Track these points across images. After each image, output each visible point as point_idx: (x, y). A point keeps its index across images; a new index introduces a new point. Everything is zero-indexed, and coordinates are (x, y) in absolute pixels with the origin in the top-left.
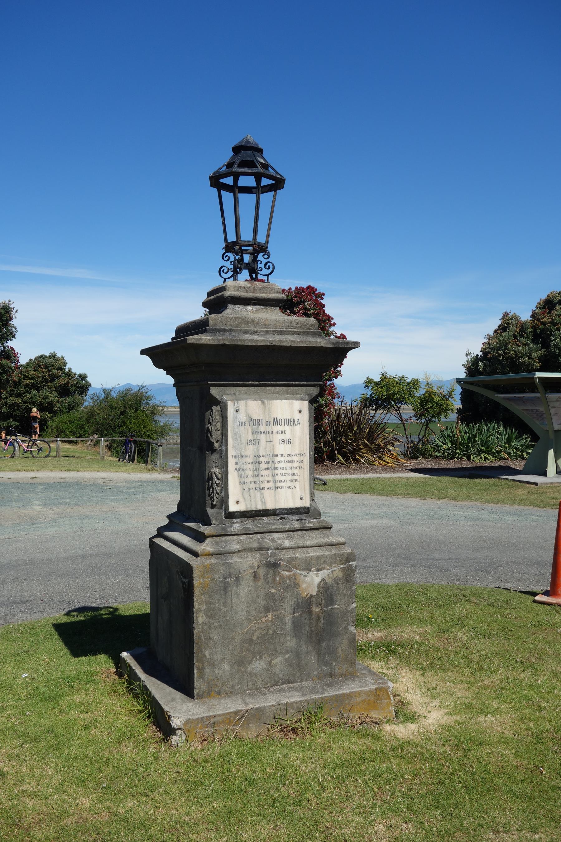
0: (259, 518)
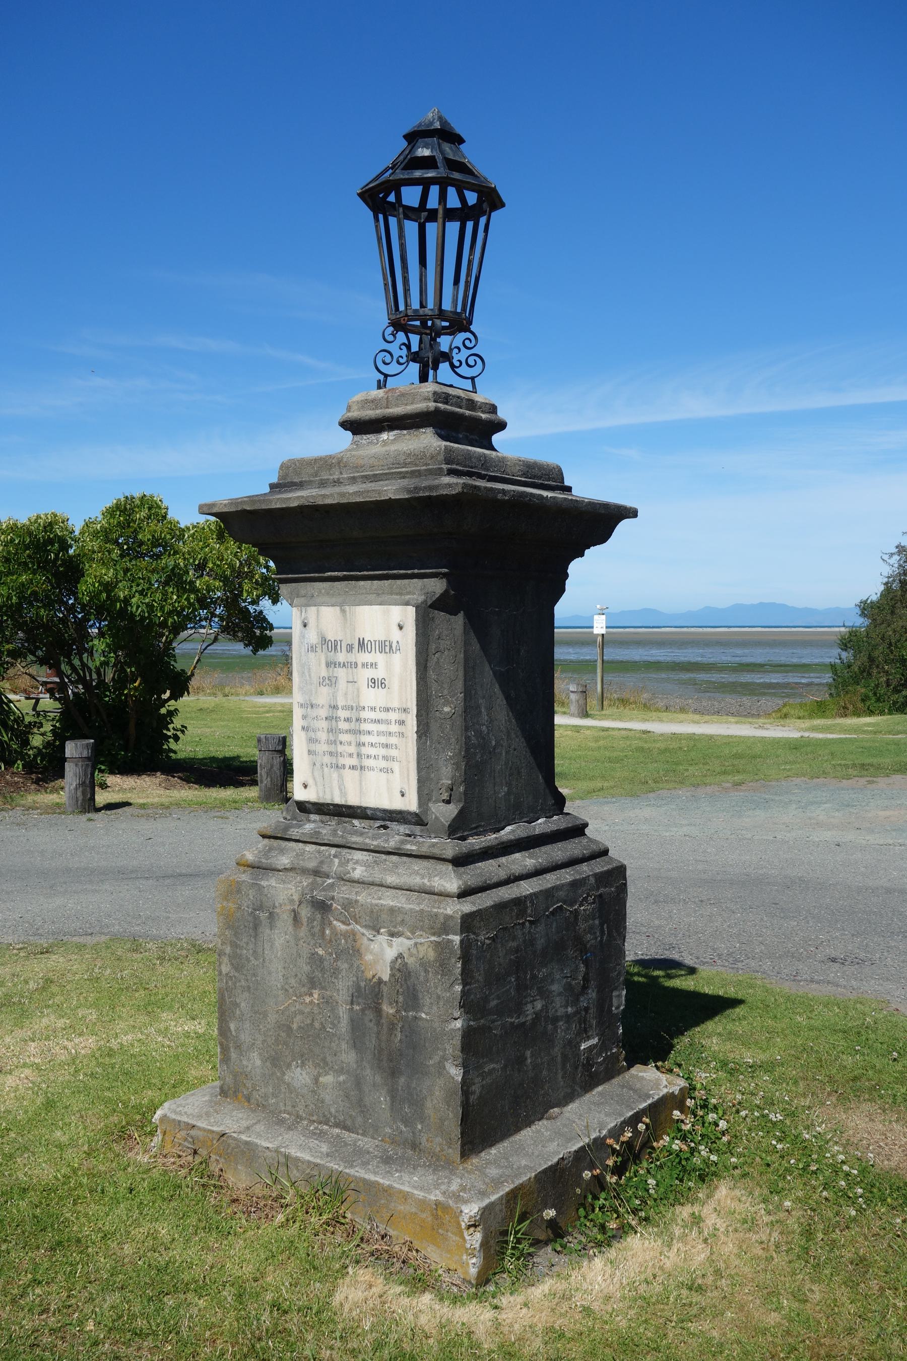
0: (347, 819)
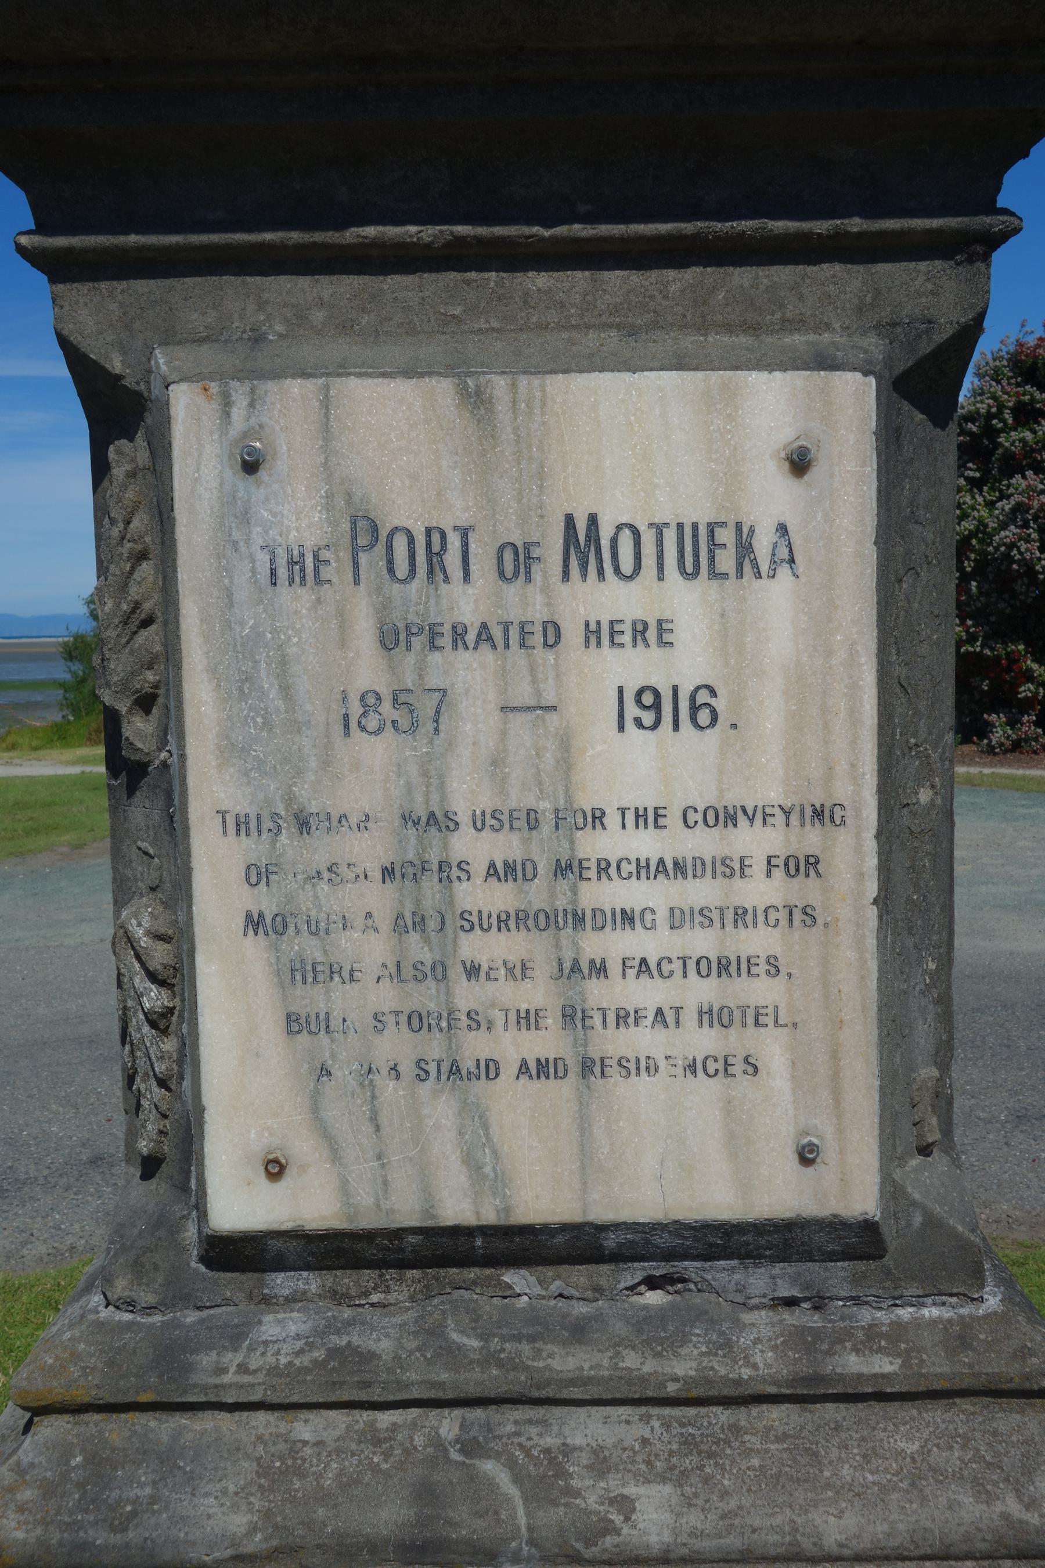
0: (473, 1273)
